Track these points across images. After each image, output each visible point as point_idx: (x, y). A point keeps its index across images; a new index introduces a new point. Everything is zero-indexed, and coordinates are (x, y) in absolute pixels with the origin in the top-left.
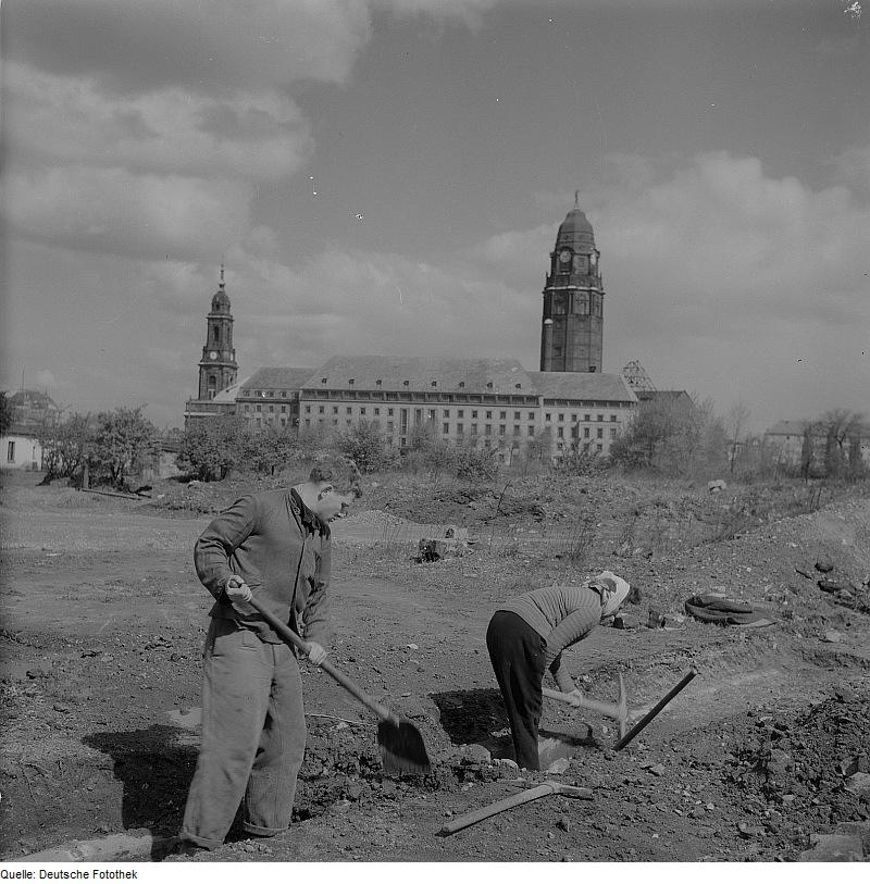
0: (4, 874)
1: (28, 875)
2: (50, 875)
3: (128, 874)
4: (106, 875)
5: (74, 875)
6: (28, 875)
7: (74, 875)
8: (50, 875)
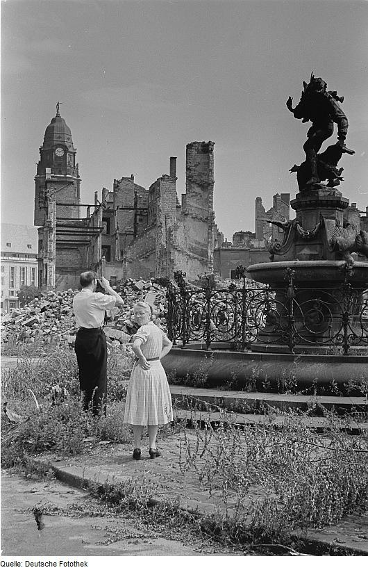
0: (3, 564)
1: (18, 564)
2: (32, 564)
3: (82, 563)
4: (68, 564)
5: (47, 564)
6: (18, 564)
7: (47, 564)
8: (32, 564)
